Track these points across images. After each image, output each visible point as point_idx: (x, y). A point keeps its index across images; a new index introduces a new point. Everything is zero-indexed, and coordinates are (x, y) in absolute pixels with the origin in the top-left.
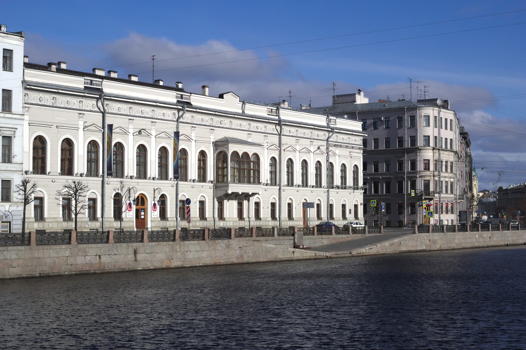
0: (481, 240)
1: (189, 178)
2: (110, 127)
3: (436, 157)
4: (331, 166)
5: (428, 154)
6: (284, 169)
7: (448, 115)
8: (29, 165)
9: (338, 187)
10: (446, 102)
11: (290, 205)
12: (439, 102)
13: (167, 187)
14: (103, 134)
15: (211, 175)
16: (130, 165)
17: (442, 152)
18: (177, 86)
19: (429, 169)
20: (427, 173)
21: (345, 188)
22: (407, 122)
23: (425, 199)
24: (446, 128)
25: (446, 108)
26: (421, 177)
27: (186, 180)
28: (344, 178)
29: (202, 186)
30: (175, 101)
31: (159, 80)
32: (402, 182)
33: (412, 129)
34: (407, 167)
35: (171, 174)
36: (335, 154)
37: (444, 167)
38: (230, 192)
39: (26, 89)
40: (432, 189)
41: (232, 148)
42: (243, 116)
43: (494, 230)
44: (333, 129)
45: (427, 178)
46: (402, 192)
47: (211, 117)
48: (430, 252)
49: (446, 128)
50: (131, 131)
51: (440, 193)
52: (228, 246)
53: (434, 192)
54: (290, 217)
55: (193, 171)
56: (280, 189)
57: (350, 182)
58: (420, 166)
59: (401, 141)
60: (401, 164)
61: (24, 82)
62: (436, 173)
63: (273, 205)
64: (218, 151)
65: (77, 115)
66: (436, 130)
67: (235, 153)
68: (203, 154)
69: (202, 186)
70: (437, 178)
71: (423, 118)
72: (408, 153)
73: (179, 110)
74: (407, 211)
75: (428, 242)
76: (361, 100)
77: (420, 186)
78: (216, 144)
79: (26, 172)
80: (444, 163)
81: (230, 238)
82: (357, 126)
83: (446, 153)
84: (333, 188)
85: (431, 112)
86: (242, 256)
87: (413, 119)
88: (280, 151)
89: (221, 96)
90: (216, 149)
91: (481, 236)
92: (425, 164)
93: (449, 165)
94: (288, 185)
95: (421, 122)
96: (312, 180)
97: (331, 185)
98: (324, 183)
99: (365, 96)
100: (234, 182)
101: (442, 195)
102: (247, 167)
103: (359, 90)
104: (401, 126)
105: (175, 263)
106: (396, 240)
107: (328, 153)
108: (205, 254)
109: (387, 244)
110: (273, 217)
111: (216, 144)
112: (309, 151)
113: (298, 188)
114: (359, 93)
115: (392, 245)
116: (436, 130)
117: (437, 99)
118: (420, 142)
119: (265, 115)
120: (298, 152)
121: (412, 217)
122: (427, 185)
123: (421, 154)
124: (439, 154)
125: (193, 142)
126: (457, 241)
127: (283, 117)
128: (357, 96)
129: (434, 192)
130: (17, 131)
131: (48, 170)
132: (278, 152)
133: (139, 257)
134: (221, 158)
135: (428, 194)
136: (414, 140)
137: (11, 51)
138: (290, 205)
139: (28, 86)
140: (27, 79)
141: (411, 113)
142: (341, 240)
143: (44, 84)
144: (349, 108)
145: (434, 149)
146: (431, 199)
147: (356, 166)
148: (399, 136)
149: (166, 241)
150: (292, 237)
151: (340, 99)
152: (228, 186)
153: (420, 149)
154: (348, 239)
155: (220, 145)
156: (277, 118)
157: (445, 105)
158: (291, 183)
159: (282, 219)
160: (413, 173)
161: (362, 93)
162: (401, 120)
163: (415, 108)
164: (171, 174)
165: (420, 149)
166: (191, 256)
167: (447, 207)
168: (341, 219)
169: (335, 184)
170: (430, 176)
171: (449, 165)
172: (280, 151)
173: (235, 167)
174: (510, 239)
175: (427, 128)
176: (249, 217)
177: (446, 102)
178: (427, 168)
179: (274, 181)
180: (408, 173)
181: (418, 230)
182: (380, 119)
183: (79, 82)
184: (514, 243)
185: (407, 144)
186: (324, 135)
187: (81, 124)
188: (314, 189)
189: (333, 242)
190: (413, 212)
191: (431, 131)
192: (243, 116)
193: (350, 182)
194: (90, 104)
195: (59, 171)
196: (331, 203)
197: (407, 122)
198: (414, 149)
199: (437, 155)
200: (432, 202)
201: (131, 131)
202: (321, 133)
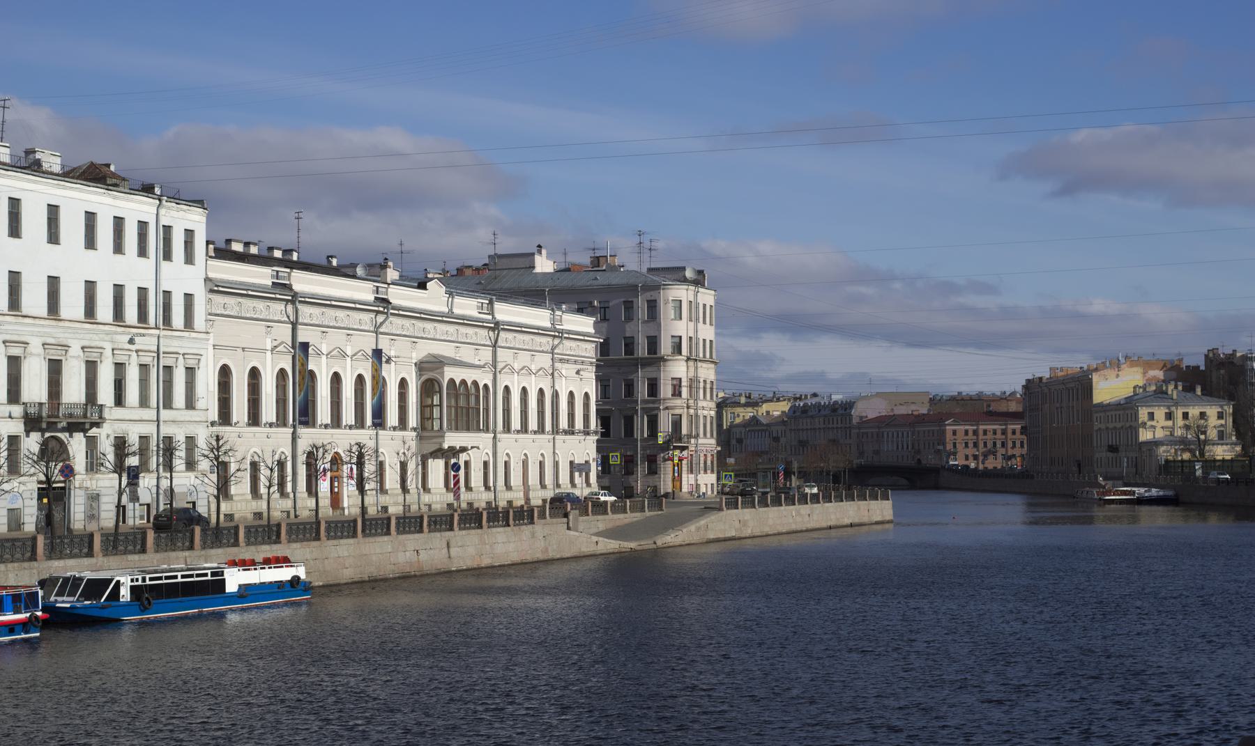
0: (799, 519)
1: (264, 421)
2: (305, 346)
3: (691, 374)
4: (556, 395)
5: (678, 369)
7: (707, 297)
8: (214, 415)
10: (701, 272)
11: (507, 464)
12: (689, 274)
14: (294, 357)
15: (413, 420)
17: (700, 364)
18: (330, 262)
19: (680, 395)
20: (678, 402)
21: (573, 433)
22: (642, 311)
23: (676, 448)
24: (704, 322)
25: (703, 286)
26: (667, 408)
27: (314, 426)
30: (371, 298)
31: (292, 250)
32: (632, 418)
33: (651, 324)
34: (642, 391)
35: (369, 421)
36: (561, 376)
37: (701, 391)
38: (446, 446)
39: (212, 291)
40: (684, 431)
41: (450, 373)
42: (448, 318)
43: (404, 532)
44: (562, 331)
45: (677, 412)
46: (632, 435)
47: (413, 321)
48: (737, 542)
49: (704, 322)
51: (697, 436)
52: (533, 535)
53: (689, 436)
54: (508, 486)
56: (495, 438)
57: (579, 424)
58: (665, 390)
59: (630, 345)
60: (630, 388)
61: (207, 280)
62: (691, 402)
63: (486, 464)
64: (424, 378)
65: (345, 337)
66: (691, 325)
67: (452, 381)
68: (586, 395)
70: (692, 411)
71: (671, 305)
72: (643, 366)
73: (378, 312)
74: (641, 469)
75: (737, 524)
76: (544, 265)
77: (665, 426)
78: (421, 367)
79: (213, 424)
80: (702, 385)
81: (451, 529)
82: (585, 324)
83: (704, 365)
84: (557, 433)
85: (682, 293)
86: (546, 550)
87: (653, 306)
88: (495, 375)
89: (422, 286)
90: (421, 375)
91: (798, 513)
92: (674, 386)
93: (708, 386)
94: (504, 432)
95: (667, 312)
96: (533, 424)
97: (556, 430)
98: (548, 427)
99: (548, 257)
100: (450, 429)
101: (701, 441)
102: (469, 407)
103: (539, 246)
104: (629, 318)
105: (486, 562)
106: (703, 522)
108: (511, 547)
109: (692, 527)
110: (487, 488)
111: (421, 367)
112: (344, 355)
113: (392, 433)
114: (540, 252)
115: (698, 529)
116: (691, 325)
117: (684, 269)
118: (665, 348)
119: (474, 313)
120: (324, 357)
121: (651, 480)
122: (677, 424)
123: (668, 369)
124: (696, 368)
125: (324, 357)
126: (771, 522)
127: (500, 317)
128: (537, 258)
129: (689, 436)
130: (203, 359)
131: (235, 420)
132: (491, 376)
133: (453, 551)
134: (429, 388)
135: (680, 440)
136: (653, 343)
137: (18, 200)
138: (507, 464)
139: (215, 287)
140: (211, 275)
141: (648, 295)
142: (618, 523)
143: (231, 282)
144: (526, 282)
145: (688, 359)
146: (683, 449)
147: (586, 395)
148: (628, 335)
149: (18, 560)
150: (565, 520)
151: (504, 260)
152: (443, 437)
153: (666, 360)
154: (627, 521)
155: (430, 368)
156: (490, 317)
157: (699, 281)
158: (507, 428)
159: (498, 488)
160: (653, 402)
161: (544, 252)
162: (629, 306)
163: (657, 287)
164: (369, 421)
165: (666, 360)
166: (499, 549)
167: (705, 462)
168: (483, 489)
170: (682, 407)
171: (708, 386)
172: (495, 375)
173: (451, 404)
174: (833, 517)
175: (678, 323)
176: (294, 493)
177: (701, 272)
178: (677, 393)
180: (644, 401)
181: (459, 524)
182: (591, 303)
183: (262, 276)
184: (839, 523)
185: (642, 350)
186: (546, 343)
188: (274, 430)
189: (610, 526)
190: (653, 471)
191: (682, 328)
192: (448, 318)
193: (579, 424)
194: (277, 309)
195: (246, 420)
196: (380, 459)
197: (642, 311)
198: (655, 359)
199: (692, 369)
200: (685, 453)
202: (544, 340)
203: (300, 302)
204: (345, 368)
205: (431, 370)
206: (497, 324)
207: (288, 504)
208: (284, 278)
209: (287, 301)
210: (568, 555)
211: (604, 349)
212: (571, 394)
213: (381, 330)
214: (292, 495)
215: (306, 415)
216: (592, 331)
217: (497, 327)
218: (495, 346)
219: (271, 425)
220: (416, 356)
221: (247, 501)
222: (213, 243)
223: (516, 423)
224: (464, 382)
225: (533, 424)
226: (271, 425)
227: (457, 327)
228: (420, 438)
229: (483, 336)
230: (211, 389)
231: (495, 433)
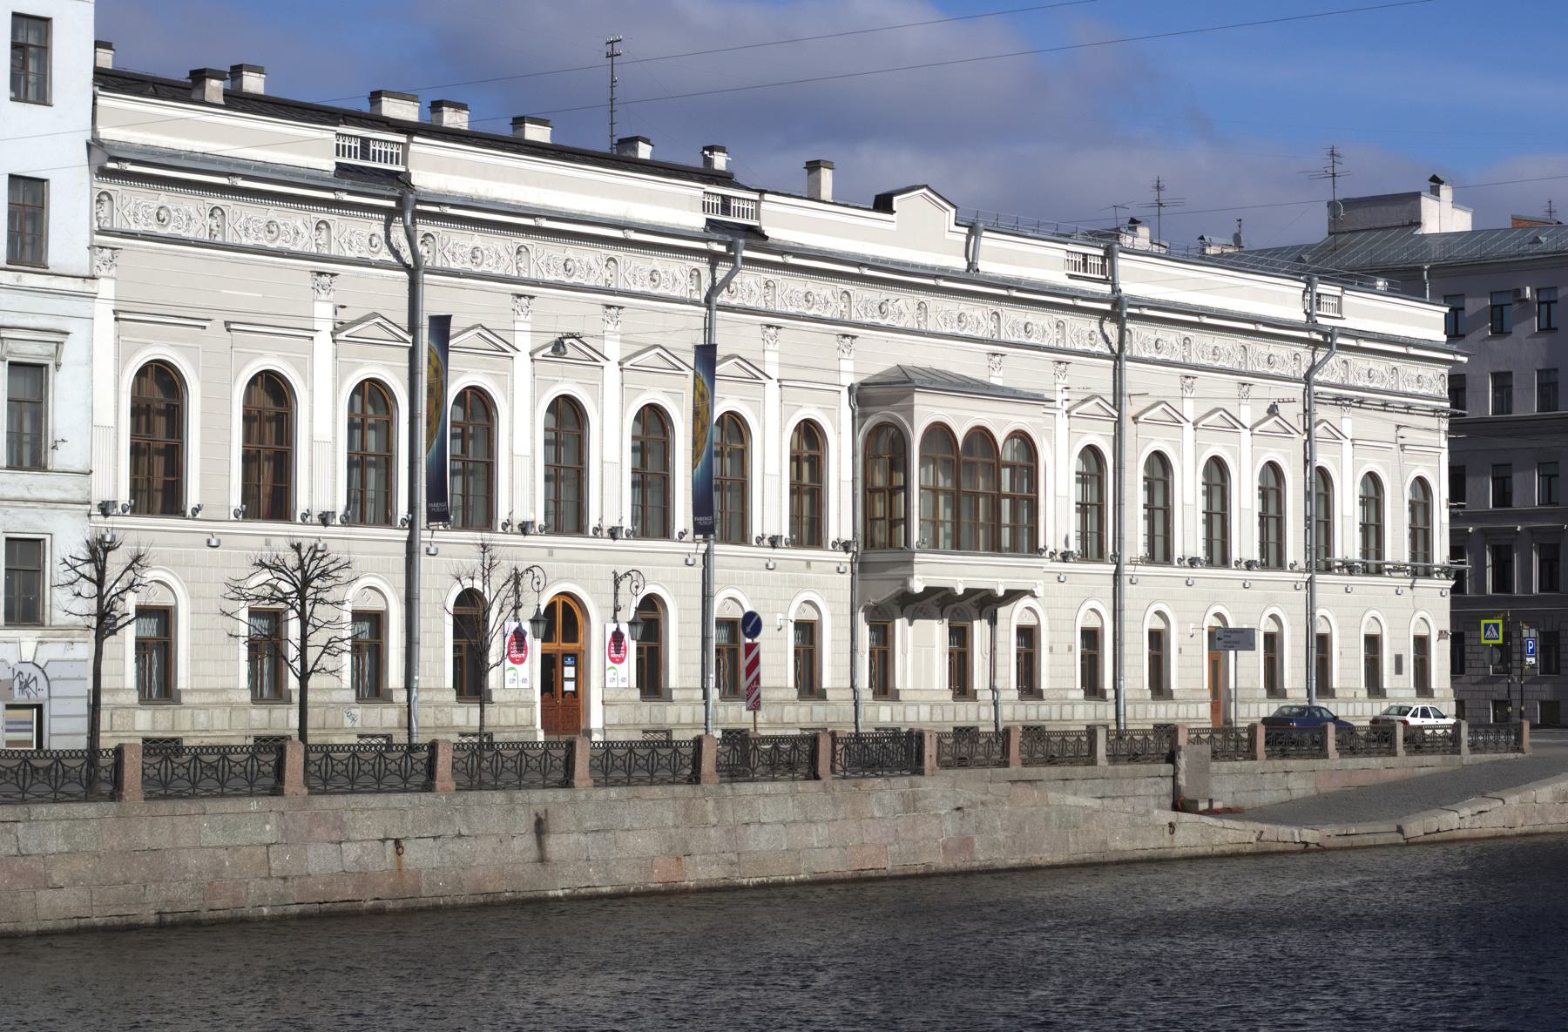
1: (756, 531)
2: (441, 325)
6: (1136, 495)
8: (115, 480)
9: (1350, 568)
11: (1157, 639)
13: (668, 569)
14: (413, 353)
15: (841, 518)
16: (521, 483)
18: (708, 162)
21: (1379, 571)
28: (1372, 530)
29: (808, 563)
30: (697, 221)
36: (1337, 436)
38: (918, 586)
39: (103, 173)
41: (927, 410)
42: (969, 284)
44: (1329, 334)
50: (524, 342)
52: (911, 804)
55: (770, 505)
56: (1117, 575)
57: (1397, 546)
61: (94, 145)
63: (1091, 638)
64: (870, 422)
65: (1051, 368)
69: (808, 563)
73: (714, 259)
76: (1443, 217)
78: (863, 396)
79: (105, 508)
86: (965, 844)
88: (1119, 424)
89: (883, 204)
90: (864, 416)
94: (1151, 559)
96: (1245, 539)
97: (1321, 559)
98: (1295, 549)
99: (1458, 202)
100: (934, 546)
102: (987, 488)
103: (1435, 179)
107: (1308, 431)
108: (817, 835)
111: (863, 396)
112: (1235, 424)
114: (1435, 192)
119: (1059, 278)
120: (1188, 427)
125: (772, 386)
127: (1128, 288)
128: (1428, 205)
131: (193, 497)
134: (884, 448)
137: (46, 21)
138: (1157, 639)
139: (112, 164)
140: (106, 133)
142: (1361, 780)
143: (176, 154)
144: (1395, 251)
147: (1421, 484)
150: (1166, 768)
154: (1392, 775)
155: (880, 399)
156: (1107, 289)
158: (1160, 550)
166: (761, 841)
169: (1338, 555)
172: (1119, 424)
176: (993, 688)
179: (1094, 543)
182: (1518, 292)
186: (1290, 358)
187: (323, 313)
188: (1255, 574)
189: (1331, 786)
192: (969, 284)
193: (1397, 546)
194: (357, 233)
196: (1321, 629)
201: (524, 342)
202: (1282, 351)
203: (1132, 316)
204: (597, 389)
205: (887, 402)
206: (1117, 301)
207: (1106, 711)
208: (745, 213)
209: (1103, 315)
210: (1059, 858)
211: (1458, 387)
212: (1373, 481)
213: (723, 298)
214: (400, 697)
215: (723, 510)
216: (1444, 338)
217: (1118, 311)
218: (1117, 358)
219: (1250, 565)
220: (850, 372)
221: (233, 707)
222: (108, 46)
223: (1189, 535)
224: (981, 435)
225: (1245, 539)
226: (1250, 565)
227: (1242, 340)
228: (862, 568)
229: (1082, 330)
230: (105, 416)
231: (1117, 560)
